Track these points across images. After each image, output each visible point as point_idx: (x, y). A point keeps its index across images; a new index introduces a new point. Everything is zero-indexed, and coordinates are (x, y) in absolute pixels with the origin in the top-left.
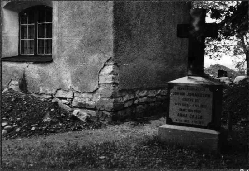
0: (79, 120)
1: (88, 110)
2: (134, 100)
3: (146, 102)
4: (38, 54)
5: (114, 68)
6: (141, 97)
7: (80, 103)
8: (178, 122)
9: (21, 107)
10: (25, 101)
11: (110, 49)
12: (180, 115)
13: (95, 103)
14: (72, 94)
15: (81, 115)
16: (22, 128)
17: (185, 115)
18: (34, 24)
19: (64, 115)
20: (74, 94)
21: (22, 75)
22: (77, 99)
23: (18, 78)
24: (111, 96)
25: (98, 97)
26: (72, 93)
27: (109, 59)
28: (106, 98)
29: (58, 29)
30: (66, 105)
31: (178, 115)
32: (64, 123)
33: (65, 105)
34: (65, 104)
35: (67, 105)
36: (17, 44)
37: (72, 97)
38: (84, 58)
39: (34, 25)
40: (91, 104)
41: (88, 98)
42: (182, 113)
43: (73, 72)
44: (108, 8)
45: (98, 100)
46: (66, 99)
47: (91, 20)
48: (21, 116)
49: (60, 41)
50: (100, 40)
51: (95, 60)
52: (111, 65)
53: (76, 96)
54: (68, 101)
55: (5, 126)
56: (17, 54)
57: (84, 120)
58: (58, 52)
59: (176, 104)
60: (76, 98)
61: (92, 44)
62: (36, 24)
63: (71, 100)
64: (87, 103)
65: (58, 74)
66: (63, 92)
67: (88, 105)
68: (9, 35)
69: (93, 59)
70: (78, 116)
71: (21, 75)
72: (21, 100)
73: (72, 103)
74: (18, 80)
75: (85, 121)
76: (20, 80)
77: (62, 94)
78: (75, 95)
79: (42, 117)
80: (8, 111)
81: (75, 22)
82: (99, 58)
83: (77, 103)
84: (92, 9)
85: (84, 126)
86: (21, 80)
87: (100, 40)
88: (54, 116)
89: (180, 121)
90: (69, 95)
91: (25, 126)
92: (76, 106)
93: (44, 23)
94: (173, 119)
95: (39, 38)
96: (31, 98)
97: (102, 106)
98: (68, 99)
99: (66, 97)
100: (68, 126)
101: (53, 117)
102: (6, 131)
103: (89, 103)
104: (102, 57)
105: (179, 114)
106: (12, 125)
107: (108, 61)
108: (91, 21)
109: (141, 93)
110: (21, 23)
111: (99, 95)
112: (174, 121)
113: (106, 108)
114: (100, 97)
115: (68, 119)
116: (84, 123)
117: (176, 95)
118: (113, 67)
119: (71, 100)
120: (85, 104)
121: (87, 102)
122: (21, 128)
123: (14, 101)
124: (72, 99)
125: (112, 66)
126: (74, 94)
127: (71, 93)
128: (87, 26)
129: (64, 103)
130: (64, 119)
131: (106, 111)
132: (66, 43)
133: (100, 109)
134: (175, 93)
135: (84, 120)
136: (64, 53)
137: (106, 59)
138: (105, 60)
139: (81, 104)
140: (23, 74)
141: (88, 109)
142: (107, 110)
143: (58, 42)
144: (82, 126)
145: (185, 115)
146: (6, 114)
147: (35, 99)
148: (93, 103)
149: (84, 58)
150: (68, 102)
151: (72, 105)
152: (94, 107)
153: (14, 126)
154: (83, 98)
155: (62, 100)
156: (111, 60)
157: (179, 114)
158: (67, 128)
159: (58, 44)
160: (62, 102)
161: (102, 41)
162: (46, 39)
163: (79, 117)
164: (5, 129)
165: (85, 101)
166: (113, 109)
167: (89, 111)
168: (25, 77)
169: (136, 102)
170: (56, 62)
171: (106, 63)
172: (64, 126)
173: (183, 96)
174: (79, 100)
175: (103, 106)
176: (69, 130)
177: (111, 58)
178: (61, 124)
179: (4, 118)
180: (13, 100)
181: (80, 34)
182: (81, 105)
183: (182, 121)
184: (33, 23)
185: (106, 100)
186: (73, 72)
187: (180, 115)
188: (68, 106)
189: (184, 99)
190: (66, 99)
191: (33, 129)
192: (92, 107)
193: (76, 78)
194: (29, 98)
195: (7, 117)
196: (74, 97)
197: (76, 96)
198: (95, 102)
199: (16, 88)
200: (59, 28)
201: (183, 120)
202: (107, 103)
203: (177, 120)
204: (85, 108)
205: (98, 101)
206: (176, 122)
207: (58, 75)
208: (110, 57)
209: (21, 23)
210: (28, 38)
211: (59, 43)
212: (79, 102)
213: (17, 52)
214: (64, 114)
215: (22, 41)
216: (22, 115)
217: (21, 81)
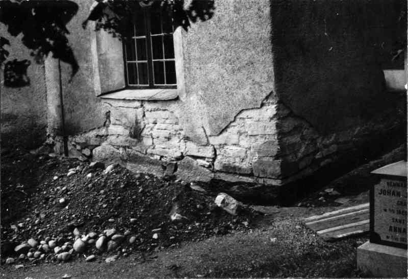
0: (227, 213)
1: (241, 177)
2: (315, 153)
3: (337, 153)
4: (155, 85)
5: (278, 109)
6: (326, 146)
7: (226, 165)
8: (390, 240)
9: (134, 197)
10: (139, 185)
11: (272, 80)
12: (393, 228)
13: (250, 165)
14: (212, 151)
15: (228, 204)
16: (138, 237)
17: (402, 230)
18: (144, 37)
19: (202, 207)
20: (215, 150)
21: (134, 122)
22: (221, 159)
23: (129, 125)
24: (276, 155)
25: (254, 156)
26: (213, 149)
27: (268, 93)
28: (268, 158)
29: (183, 47)
30: (205, 169)
31: (391, 229)
32: (203, 222)
33: (202, 168)
34: (204, 166)
35: (207, 168)
36: (122, 70)
37: (213, 156)
38: (227, 93)
39: (145, 39)
40: (244, 167)
41: (239, 158)
42: (398, 227)
43: (212, 116)
44: (262, 10)
45: (256, 160)
46: (203, 158)
47: (235, 31)
48: (135, 213)
49: (187, 66)
50: (252, 63)
51: (247, 96)
52: (272, 104)
53: (219, 155)
54: (207, 161)
55: (113, 235)
56: (123, 85)
57: (234, 212)
58: (186, 83)
59: (385, 210)
60: (219, 158)
61: (239, 69)
62: (148, 36)
63: (211, 160)
64: (238, 166)
65: (189, 119)
66: (198, 148)
67: (240, 169)
68: (108, 56)
69: (243, 94)
70: (224, 207)
71: (132, 120)
72: (135, 185)
73: (213, 164)
74: (129, 128)
75: (236, 214)
76: (131, 128)
77: (197, 151)
78: (217, 153)
79: (168, 212)
80: (115, 207)
81: (210, 34)
82: (253, 93)
83: (222, 165)
84: (235, 11)
85: (234, 224)
86: (133, 129)
87: (252, 63)
88: (186, 209)
89: (393, 239)
90: (209, 153)
91: (142, 233)
92: (221, 170)
93: (161, 34)
94: (381, 235)
95: (154, 59)
96: (149, 179)
97: (262, 171)
98: (206, 159)
99: (204, 156)
100: (208, 226)
101: (185, 211)
102: (114, 243)
103: (241, 166)
104: (257, 92)
105: (391, 227)
106: (122, 232)
107: (267, 98)
108: (235, 32)
109: (326, 139)
110: (126, 60)
111: (256, 153)
112: (383, 238)
113: (268, 174)
114: (257, 155)
115: (209, 213)
116: (234, 219)
117: (384, 194)
118: (276, 107)
119: (211, 160)
120: (235, 168)
121: (237, 164)
122: (137, 236)
123: (124, 187)
124: (214, 159)
125: (276, 106)
126: (215, 150)
127: (210, 149)
128: (229, 40)
129: (202, 166)
130: (201, 214)
131: (269, 178)
132: (197, 68)
133: (259, 175)
134: (383, 192)
135: (234, 212)
136: (196, 85)
137: (264, 95)
138: (262, 96)
139: (227, 167)
140: (134, 119)
141: (240, 175)
142: (270, 176)
143: (185, 67)
144: (231, 225)
145: (402, 230)
146: (113, 212)
147: (155, 180)
148: (247, 165)
149: (227, 93)
150: (208, 164)
151: (213, 169)
152: (250, 172)
153: (125, 233)
154: (230, 157)
155: (198, 160)
156: (272, 95)
157: (391, 227)
158: (207, 230)
159: (185, 70)
160: (197, 164)
161: (255, 64)
162: (166, 62)
163: (225, 209)
164: (114, 240)
165: (234, 163)
166: (280, 176)
167: (241, 179)
168: (139, 125)
169: (318, 156)
170: (184, 101)
171: (265, 102)
172: (203, 227)
173: (398, 198)
174: (225, 161)
175: (264, 171)
176: (210, 233)
177: (272, 93)
178: (197, 224)
179: (110, 220)
180: (122, 186)
181: (219, 54)
182: (229, 169)
183: (397, 239)
184: (144, 35)
185: (269, 161)
186: (212, 116)
187: (393, 228)
188: (207, 170)
189: (399, 203)
190: (203, 158)
191: (155, 236)
192: (246, 172)
193: (218, 126)
194: (146, 179)
195: (116, 217)
196: (215, 155)
197: (219, 155)
198: (251, 164)
199: (127, 141)
200: (185, 45)
201: (399, 237)
202: (270, 166)
203: (388, 237)
204: (236, 174)
205: (256, 163)
206: (388, 240)
207: (189, 121)
208: (270, 91)
209: (126, 60)
210: (138, 60)
211: (186, 70)
212: (225, 164)
213: (124, 83)
214: (201, 204)
215: (129, 64)
216: (138, 211)
217: (132, 130)
